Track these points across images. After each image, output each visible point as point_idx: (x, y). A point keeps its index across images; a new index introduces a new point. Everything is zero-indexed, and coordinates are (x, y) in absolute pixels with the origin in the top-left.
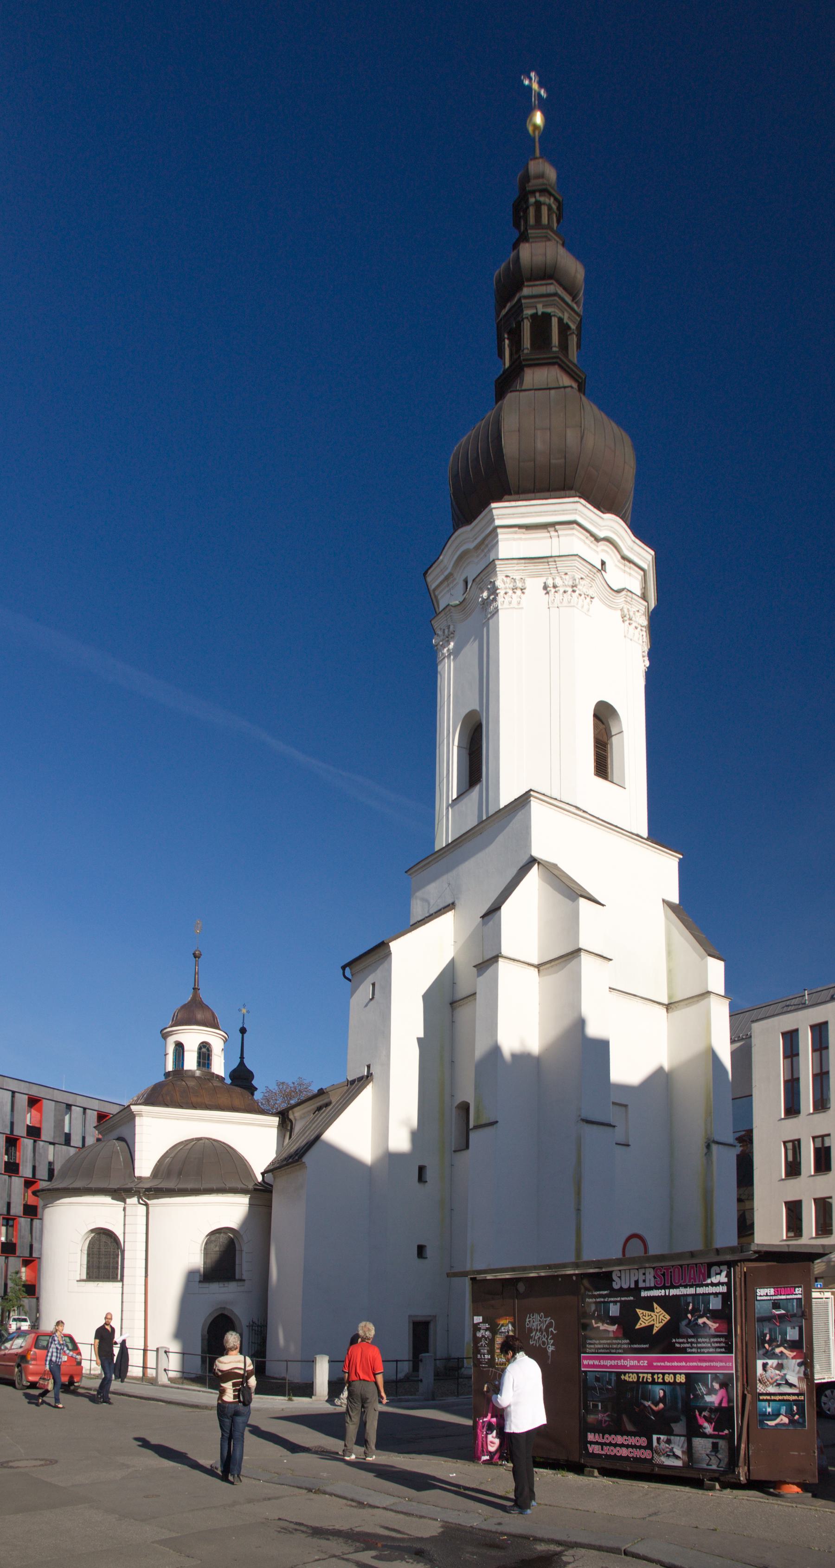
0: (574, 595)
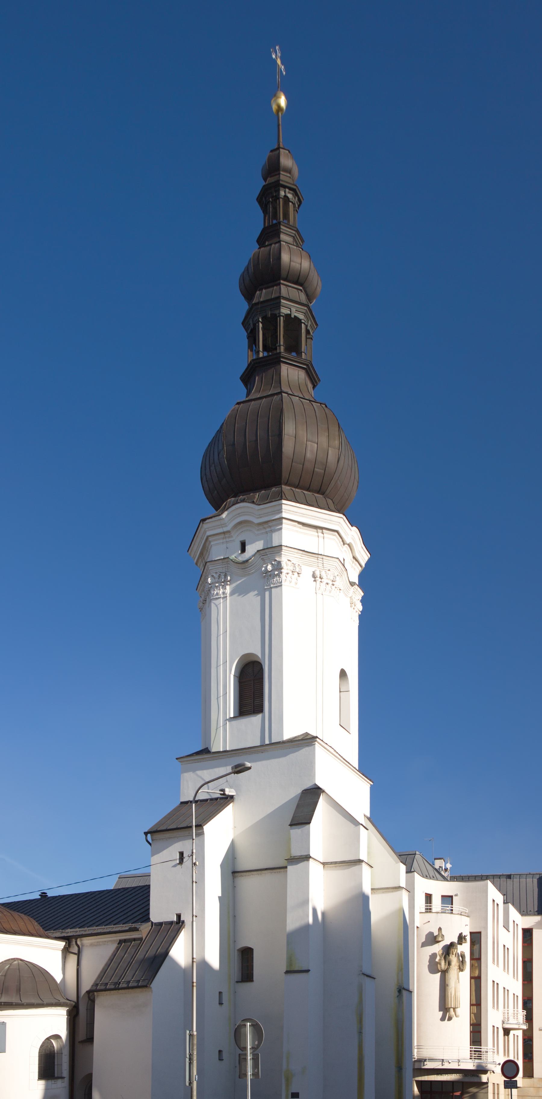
0: (333, 587)
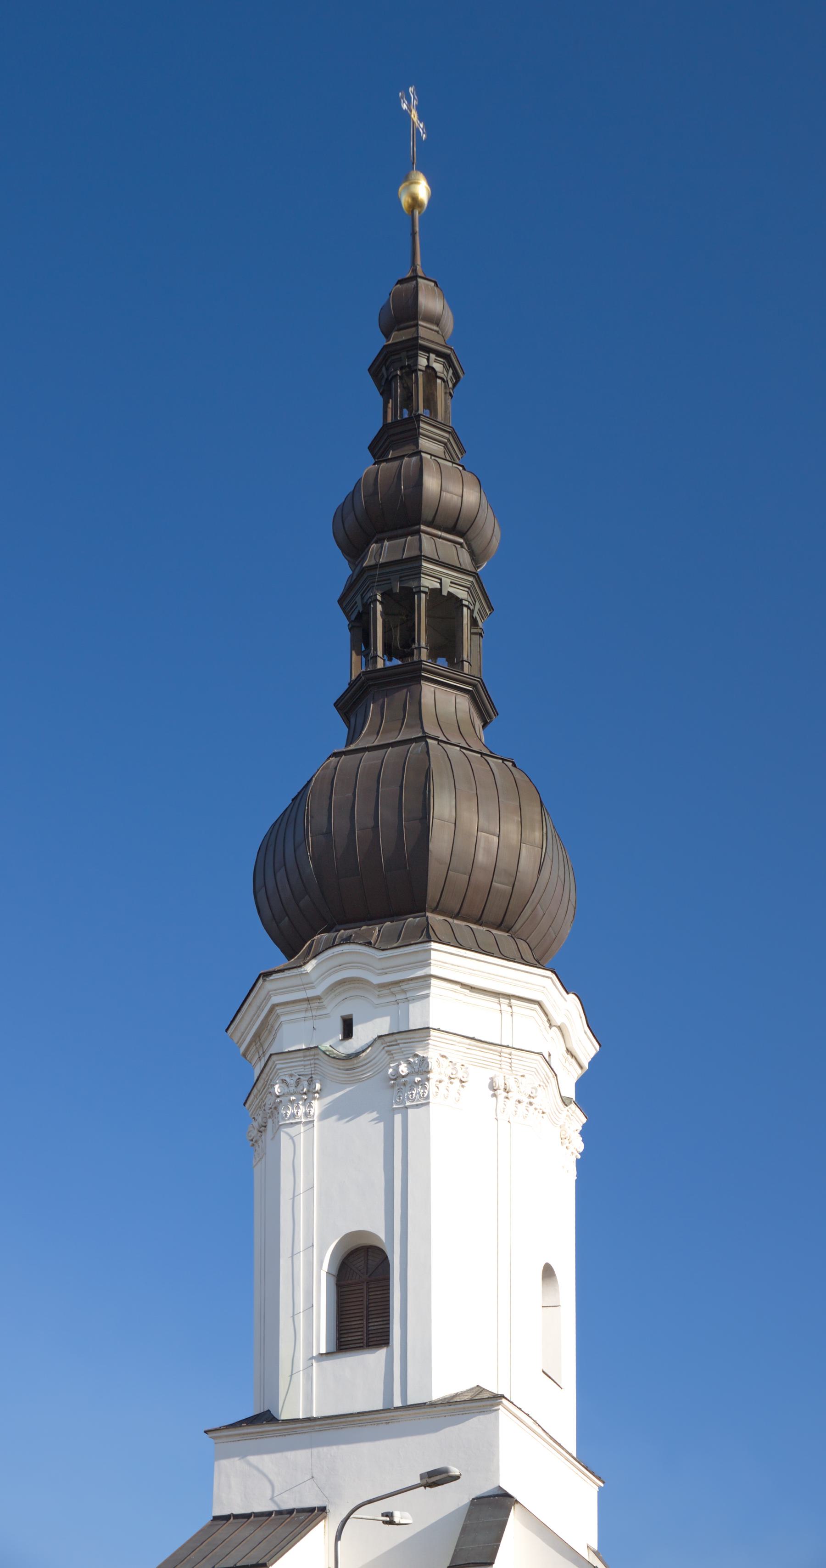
0: (531, 1108)
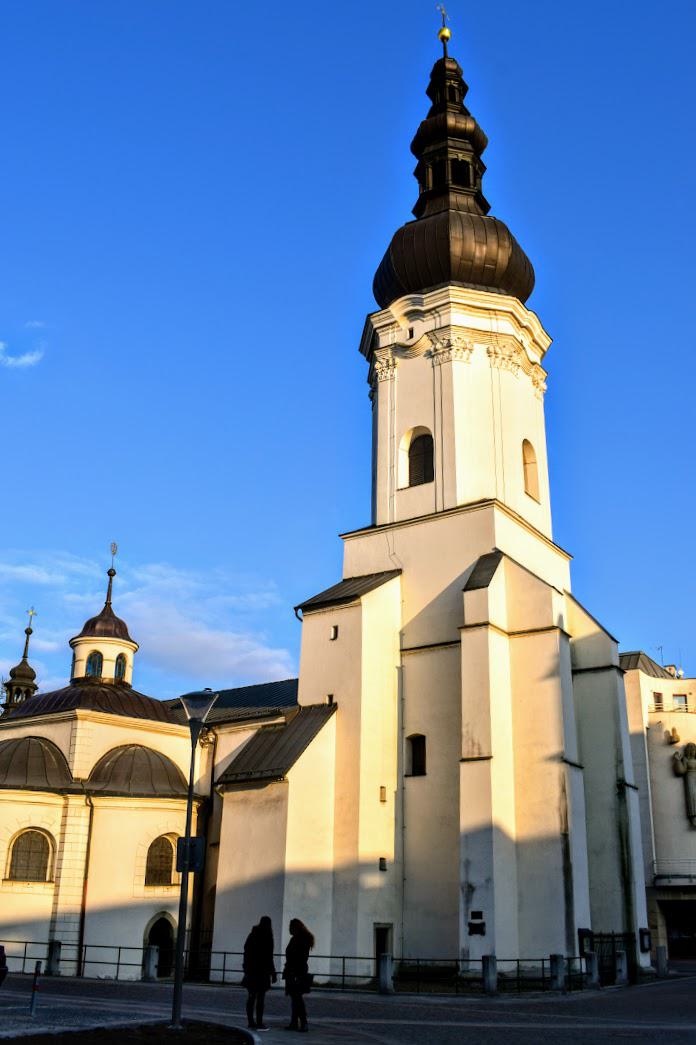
0: (510, 362)
